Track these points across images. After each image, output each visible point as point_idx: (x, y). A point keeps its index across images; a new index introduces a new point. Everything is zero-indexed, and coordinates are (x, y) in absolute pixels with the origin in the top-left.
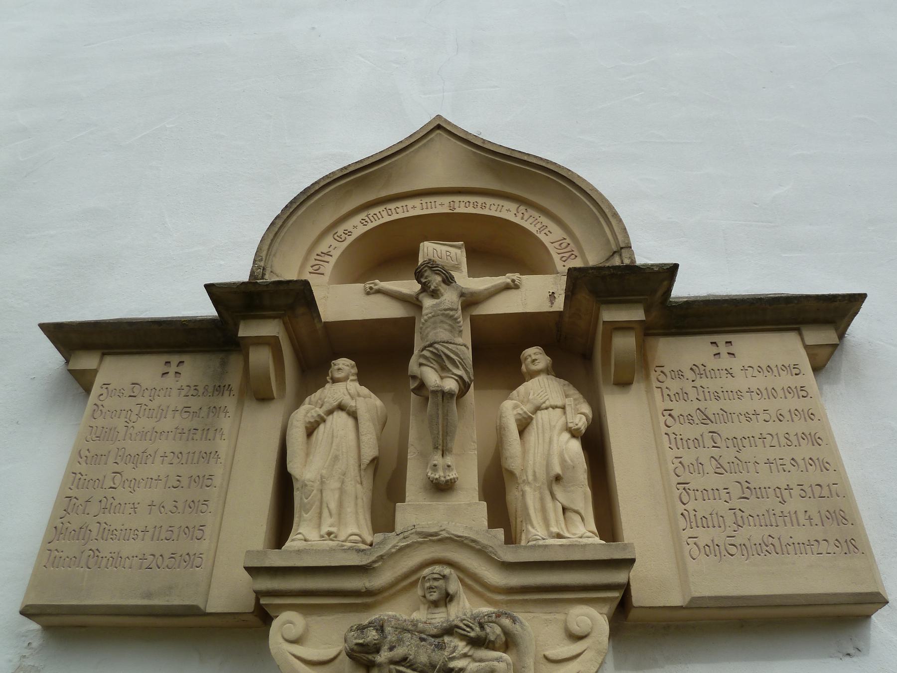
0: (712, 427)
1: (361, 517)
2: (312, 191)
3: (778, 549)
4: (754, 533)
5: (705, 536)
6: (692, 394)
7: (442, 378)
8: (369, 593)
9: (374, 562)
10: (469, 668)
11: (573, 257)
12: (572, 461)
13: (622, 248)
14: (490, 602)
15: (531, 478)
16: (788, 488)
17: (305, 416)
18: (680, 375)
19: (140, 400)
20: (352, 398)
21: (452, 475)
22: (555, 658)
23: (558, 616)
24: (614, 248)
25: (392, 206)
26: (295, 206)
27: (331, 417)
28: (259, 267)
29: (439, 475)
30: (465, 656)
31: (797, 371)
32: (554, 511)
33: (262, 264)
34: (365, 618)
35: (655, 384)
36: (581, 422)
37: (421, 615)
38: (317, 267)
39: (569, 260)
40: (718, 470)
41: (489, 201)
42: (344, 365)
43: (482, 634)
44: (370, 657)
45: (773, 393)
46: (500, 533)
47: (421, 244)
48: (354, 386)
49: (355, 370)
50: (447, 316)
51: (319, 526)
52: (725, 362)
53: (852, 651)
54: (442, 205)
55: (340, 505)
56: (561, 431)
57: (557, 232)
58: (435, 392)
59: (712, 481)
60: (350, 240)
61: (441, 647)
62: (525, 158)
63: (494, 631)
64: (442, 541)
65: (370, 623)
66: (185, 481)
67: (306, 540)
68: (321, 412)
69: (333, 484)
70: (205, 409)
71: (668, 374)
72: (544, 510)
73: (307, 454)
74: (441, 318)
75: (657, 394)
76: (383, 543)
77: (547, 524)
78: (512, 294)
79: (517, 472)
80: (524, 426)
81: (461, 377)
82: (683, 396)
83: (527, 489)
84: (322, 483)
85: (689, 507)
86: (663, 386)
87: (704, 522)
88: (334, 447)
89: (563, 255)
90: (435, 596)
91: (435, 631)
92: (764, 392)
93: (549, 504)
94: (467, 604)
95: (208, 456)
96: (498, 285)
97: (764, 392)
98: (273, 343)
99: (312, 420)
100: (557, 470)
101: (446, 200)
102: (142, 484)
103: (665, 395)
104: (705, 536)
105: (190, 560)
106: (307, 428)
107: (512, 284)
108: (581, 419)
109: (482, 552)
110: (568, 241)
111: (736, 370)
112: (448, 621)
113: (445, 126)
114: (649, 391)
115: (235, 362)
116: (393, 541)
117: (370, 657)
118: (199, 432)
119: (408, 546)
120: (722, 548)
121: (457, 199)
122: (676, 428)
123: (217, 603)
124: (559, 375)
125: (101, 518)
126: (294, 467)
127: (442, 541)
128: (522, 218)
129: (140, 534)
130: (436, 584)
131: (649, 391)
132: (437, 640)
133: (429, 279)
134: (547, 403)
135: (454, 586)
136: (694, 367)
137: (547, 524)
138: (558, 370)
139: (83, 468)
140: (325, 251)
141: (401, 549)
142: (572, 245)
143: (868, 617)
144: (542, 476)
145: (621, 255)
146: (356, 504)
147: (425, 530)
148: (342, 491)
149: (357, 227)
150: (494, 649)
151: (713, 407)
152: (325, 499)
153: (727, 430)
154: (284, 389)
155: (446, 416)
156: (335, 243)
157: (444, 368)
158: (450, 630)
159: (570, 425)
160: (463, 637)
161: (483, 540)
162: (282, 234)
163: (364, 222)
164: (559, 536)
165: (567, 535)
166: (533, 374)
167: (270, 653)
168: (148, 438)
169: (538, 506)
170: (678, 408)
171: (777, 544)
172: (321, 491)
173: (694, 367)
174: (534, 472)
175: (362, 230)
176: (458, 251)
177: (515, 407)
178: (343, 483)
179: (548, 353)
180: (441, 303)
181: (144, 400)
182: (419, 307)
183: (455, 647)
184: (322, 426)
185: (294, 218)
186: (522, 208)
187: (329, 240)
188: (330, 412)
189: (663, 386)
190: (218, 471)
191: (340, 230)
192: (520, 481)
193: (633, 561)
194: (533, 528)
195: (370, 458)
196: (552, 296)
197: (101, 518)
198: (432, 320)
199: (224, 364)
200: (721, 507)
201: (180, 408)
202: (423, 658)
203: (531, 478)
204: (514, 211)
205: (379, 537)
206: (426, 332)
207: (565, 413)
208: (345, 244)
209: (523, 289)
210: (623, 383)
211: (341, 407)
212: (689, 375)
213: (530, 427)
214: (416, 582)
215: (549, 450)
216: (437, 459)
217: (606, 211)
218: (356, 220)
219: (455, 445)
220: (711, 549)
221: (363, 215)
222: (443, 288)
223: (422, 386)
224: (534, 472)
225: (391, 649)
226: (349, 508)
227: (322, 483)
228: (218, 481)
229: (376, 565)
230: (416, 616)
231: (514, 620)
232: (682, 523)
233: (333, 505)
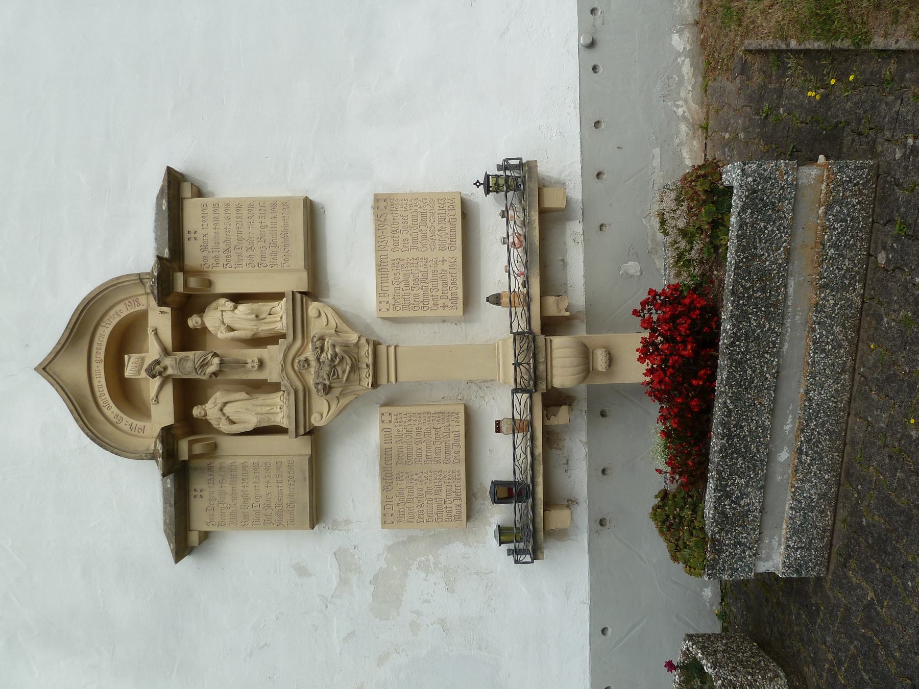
0: (232, 248)
1: (272, 397)
2: (93, 436)
3: (286, 233)
4: (280, 241)
5: (280, 260)
6: (216, 254)
7: (212, 365)
8: (304, 390)
9: (293, 388)
10: (331, 353)
11: (137, 300)
12: (249, 310)
13: (140, 278)
14: (307, 345)
15: (256, 327)
16: (261, 222)
17: (226, 425)
18: (205, 258)
19: (216, 505)
20: (216, 405)
21: (256, 360)
22: (326, 323)
23: (312, 319)
24: (139, 281)
25: (98, 394)
26: (104, 444)
27: (226, 414)
28: (146, 456)
29: (256, 365)
30: (326, 354)
31: (205, 205)
32: (270, 319)
33: (144, 455)
34: (314, 390)
35: (210, 269)
36: (230, 305)
37: (312, 370)
38: (140, 430)
39: (140, 302)
40: (253, 249)
41: (96, 341)
42: (196, 412)
43: (319, 348)
44: (327, 387)
45: (216, 219)
46: (281, 341)
47: (126, 377)
48: (209, 405)
49: (200, 406)
50: (179, 363)
51: (277, 413)
52: (199, 236)
53: (323, 210)
54: (98, 367)
55: (268, 405)
56: (234, 313)
57: (121, 307)
58: (220, 367)
59: (257, 252)
60: (121, 414)
61: (324, 362)
62: (73, 321)
63: (318, 344)
64: (285, 362)
65: (316, 388)
66: (257, 474)
67: (283, 418)
68: (224, 419)
69: (259, 409)
70: (221, 473)
71: (205, 263)
72: (269, 323)
73: (244, 422)
74: (180, 365)
75: (215, 269)
76: (285, 386)
77: (276, 322)
78: (160, 332)
79: (253, 333)
80: (231, 329)
81: (212, 356)
82: (216, 258)
83: (260, 329)
84: (258, 414)
85: (268, 264)
86: (211, 266)
87: (275, 259)
88: (242, 411)
89: (136, 305)
90: (306, 365)
91: (319, 365)
92: (215, 222)
93: (267, 320)
94: (309, 353)
95: (244, 467)
96: (155, 337)
97: (215, 222)
98: (191, 443)
99: (228, 422)
100: (253, 316)
101: (94, 365)
102: (258, 493)
103: (216, 266)
104: (280, 260)
105: (290, 466)
106: (232, 424)
107: (154, 332)
108: (228, 304)
109: (289, 348)
110: (127, 302)
111: (204, 232)
112: (315, 360)
113: (44, 365)
114: (213, 272)
115: (195, 463)
116: (285, 382)
117: (327, 387)
118: (233, 473)
119: (287, 376)
120: (285, 254)
121: (94, 359)
122: (233, 263)
123: (308, 451)
124: (203, 311)
125: (273, 507)
126: (250, 427)
127: (285, 362)
128: (110, 324)
129: (280, 488)
130: (302, 365)
131: (213, 272)
132: (321, 364)
133: (157, 371)
134: (221, 318)
135: (302, 358)
136: (202, 250)
137: (276, 322)
138: (201, 311)
139: (250, 523)
140: (129, 427)
141: (288, 378)
142: (130, 300)
143: (311, 200)
144: (255, 323)
145: (143, 279)
146: (267, 399)
147: (281, 369)
148: (261, 406)
149: (112, 411)
150: (324, 344)
151: (222, 246)
152: (265, 412)
153: (234, 242)
154: (211, 438)
155: (232, 362)
156: (124, 422)
157: (207, 364)
158: (318, 359)
159: (232, 309)
160: (321, 355)
161: (285, 347)
162: (123, 448)
163: (109, 408)
164: (281, 318)
165: (281, 314)
166: (203, 323)
167: (324, 426)
168: (235, 496)
169: (268, 325)
170: (222, 260)
171: (285, 232)
172: (262, 414)
173: (202, 250)
174: (253, 326)
175: (115, 409)
176: (132, 358)
177: (221, 332)
178: (257, 405)
179: (191, 316)
180: (171, 365)
181: (216, 503)
182: (169, 376)
183: (324, 357)
184: (230, 418)
185: (112, 444)
186: (102, 324)
187: (122, 425)
188: (224, 414)
189: (211, 266)
190: (252, 461)
191: (115, 420)
192: (257, 331)
193: (293, 291)
194: (277, 327)
195: (247, 395)
196: (162, 312)
197: (273, 507)
198: (181, 369)
199: (196, 469)
200: (268, 251)
201: (220, 485)
202: (328, 368)
203: (256, 327)
204: (105, 328)
205: (283, 388)
206: (186, 371)
207: (225, 311)
208: (124, 417)
209: (157, 326)
210: (210, 283)
211: (221, 410)
212: (206, 253)
213: (232, 327)
214: (300, 373)
215: (243, 319)
216: (249, 366)
217: (115, 282)
218: (108, 413)
219: (243, 358)
220: (286, 258)
221: (105, 410)
222: (162, 364)
223: (215, 374)
224: (253, 326)
225: (325, 380)
226: (269, 402)
227: (258, 414)
228: (256, 460)
229: (294, 388)
230: (313, 372)
231: (314, 337)
232: (275, 268)
233: (268, 408)
